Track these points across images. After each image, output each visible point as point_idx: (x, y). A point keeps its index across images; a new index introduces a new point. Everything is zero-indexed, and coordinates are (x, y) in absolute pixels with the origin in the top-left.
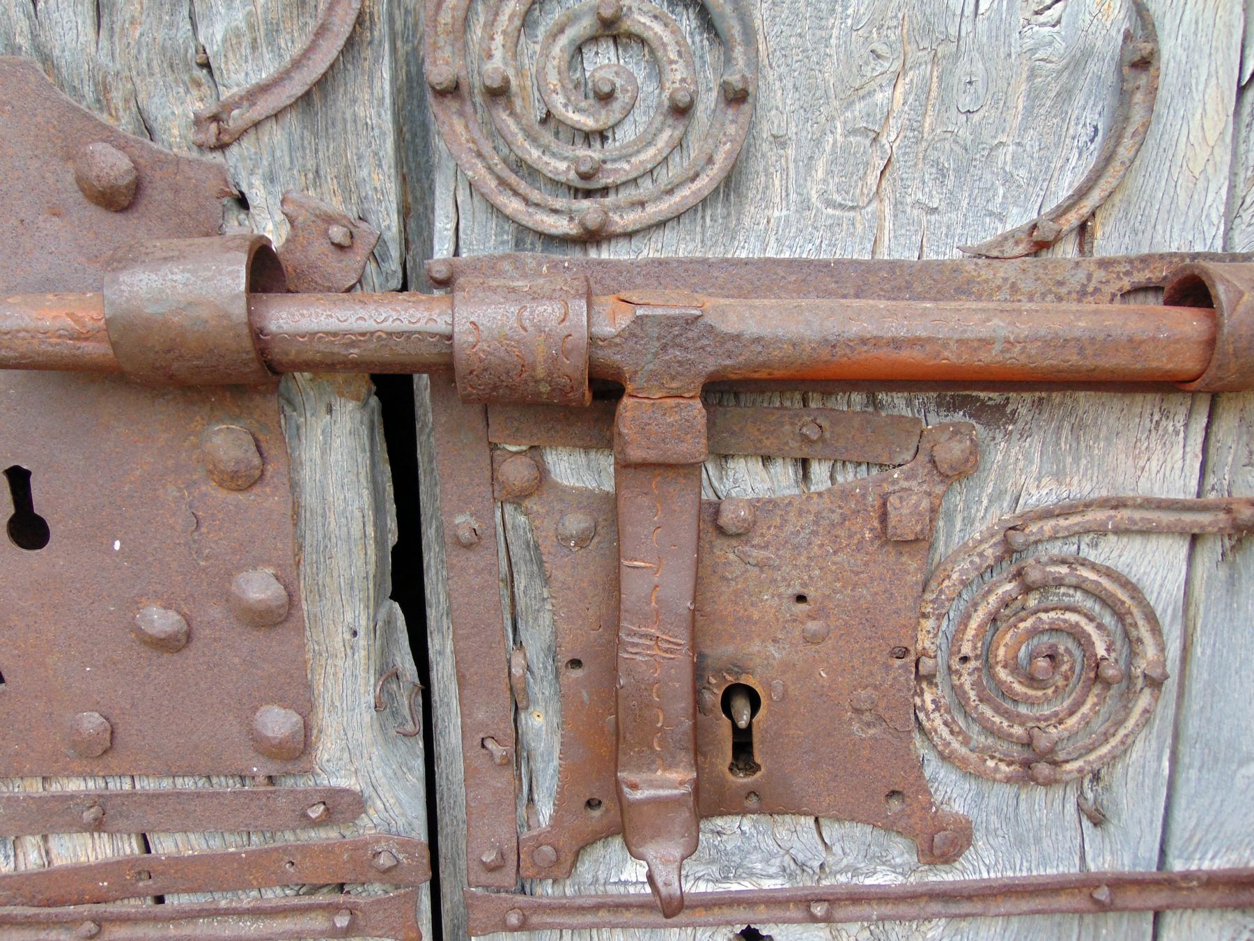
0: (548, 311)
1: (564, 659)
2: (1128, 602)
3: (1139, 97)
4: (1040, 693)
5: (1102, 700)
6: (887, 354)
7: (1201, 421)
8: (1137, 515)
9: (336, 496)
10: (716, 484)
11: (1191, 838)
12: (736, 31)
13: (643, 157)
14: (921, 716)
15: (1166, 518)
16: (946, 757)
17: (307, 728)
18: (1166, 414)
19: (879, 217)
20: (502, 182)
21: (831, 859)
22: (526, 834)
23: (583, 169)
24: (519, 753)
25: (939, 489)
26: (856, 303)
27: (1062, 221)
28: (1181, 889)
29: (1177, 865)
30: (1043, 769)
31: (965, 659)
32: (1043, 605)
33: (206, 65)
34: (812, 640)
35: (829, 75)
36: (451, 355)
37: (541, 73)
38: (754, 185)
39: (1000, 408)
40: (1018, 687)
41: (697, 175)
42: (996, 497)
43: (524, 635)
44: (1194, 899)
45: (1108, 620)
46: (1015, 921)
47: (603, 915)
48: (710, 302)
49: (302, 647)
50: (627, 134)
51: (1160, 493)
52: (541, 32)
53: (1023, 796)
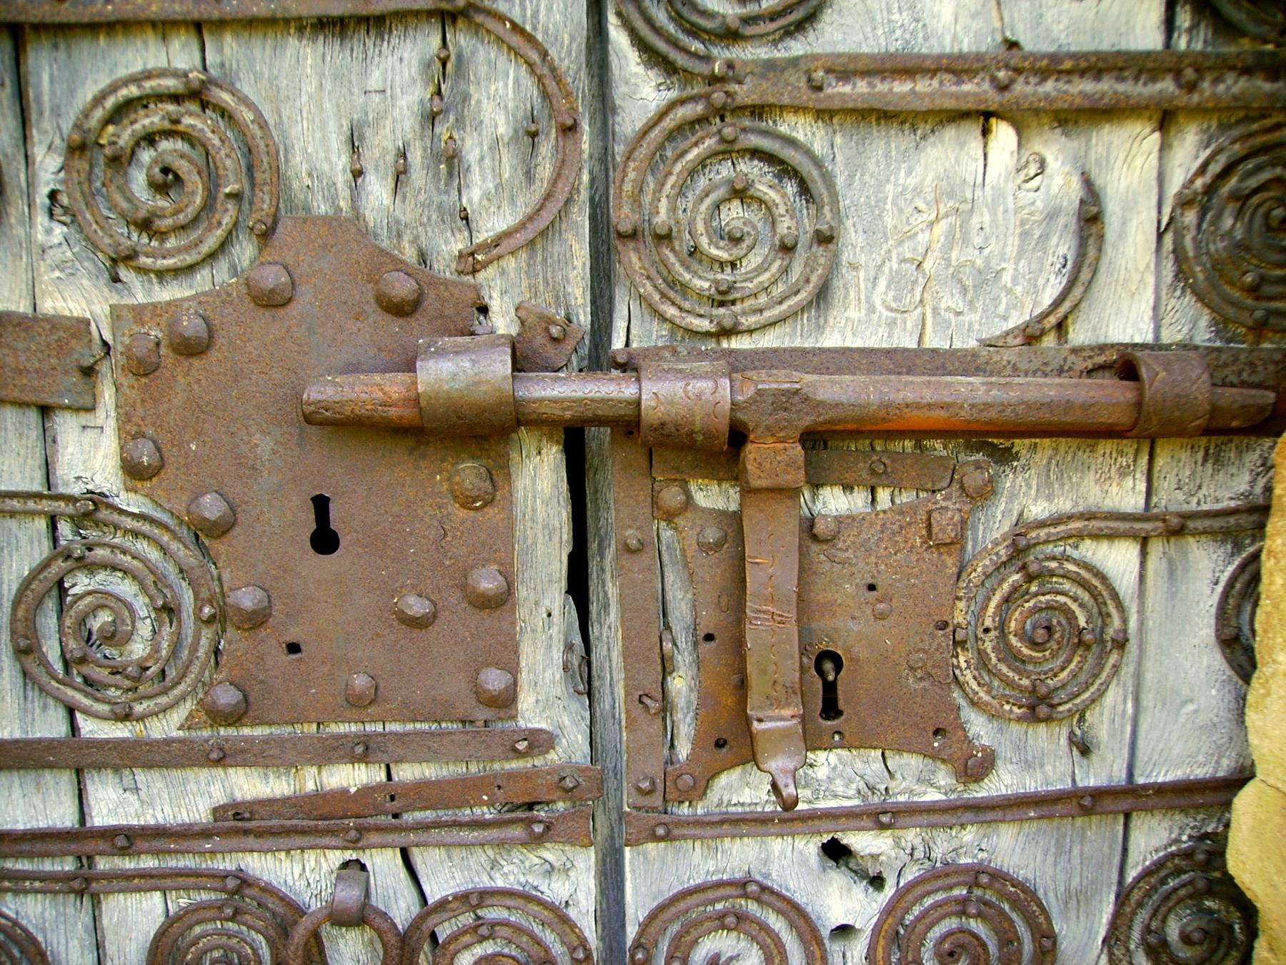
1: (701, 634)
2: (1100, 587)
3: (1091, 241)
4: (1040, 655)
5: (1084, 659)
7: (1144, 460)
8: (1102, 524)
10: (810, 505)
11: (1150, 759)
13: (761, 278)
14: (957, 672)
16: (974, 704)
17: (515, 684)
20: (663, 295)
21: (892, 784)
22: (670, 768)
23: (721, 288)
24: (666, 706)
25: (967, 508)
26: (910, 378)
27: (1045, 322)
28: (1141, 796)
29: (1140, 780)
30: (1043, 710)
31: (987, 630)
32: (1042, 590)
33: (466, 218)
34: (880, 617)
35: (889, 221)
36: (639, 415)
37: (692, 223)
38: (837, 294)
39: (1009, 449)
40: (1025, 651)
41: (798, 291)
44: (1150, 803)
45: (1086, 597)
49: (514, 624)
53: (1030, 732)
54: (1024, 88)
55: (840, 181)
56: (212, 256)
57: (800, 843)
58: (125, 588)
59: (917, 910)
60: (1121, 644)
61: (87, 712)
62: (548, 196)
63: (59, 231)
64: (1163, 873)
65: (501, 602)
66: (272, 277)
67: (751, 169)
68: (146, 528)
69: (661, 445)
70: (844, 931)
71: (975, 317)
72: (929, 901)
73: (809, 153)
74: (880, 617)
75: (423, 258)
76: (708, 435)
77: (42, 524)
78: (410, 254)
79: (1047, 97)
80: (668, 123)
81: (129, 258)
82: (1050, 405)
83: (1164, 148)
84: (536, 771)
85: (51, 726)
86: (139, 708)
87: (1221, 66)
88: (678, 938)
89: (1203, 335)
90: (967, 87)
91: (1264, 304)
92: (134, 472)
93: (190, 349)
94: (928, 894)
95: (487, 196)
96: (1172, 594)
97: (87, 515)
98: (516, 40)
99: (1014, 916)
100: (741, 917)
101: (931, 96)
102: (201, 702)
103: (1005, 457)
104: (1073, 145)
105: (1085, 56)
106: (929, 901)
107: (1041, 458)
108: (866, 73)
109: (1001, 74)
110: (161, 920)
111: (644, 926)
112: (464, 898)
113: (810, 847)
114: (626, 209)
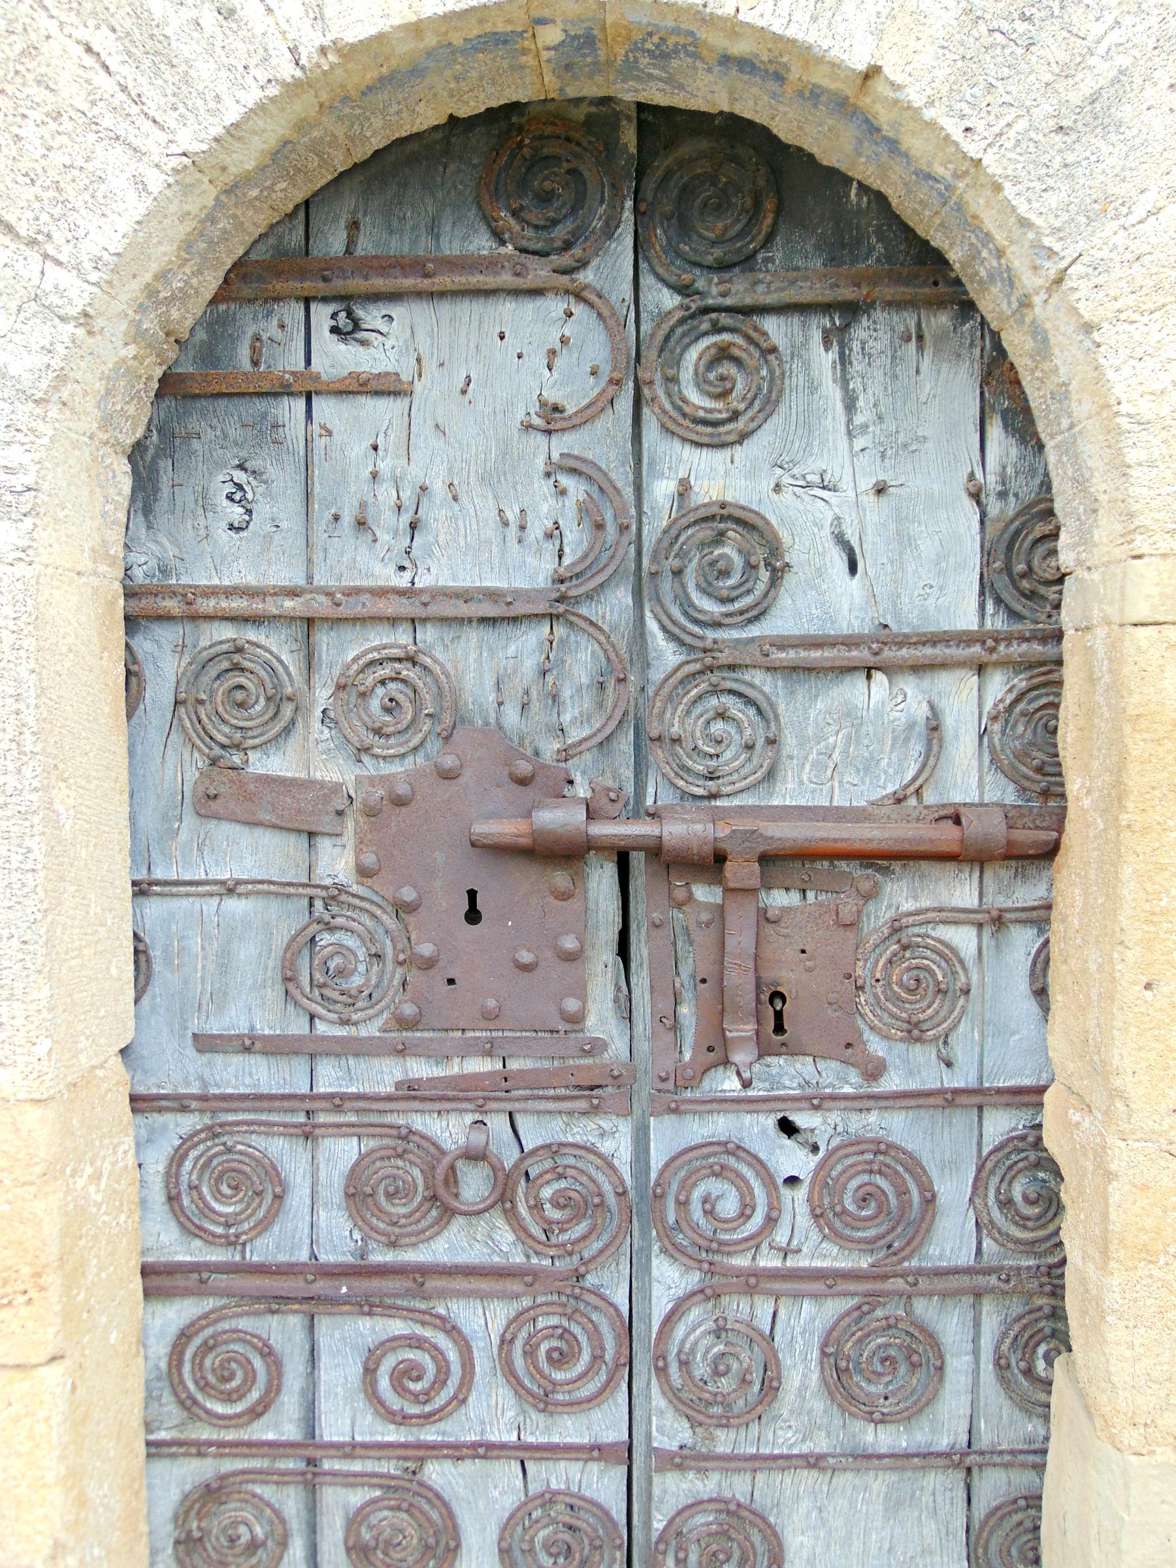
0: (699, 827)
6: (831, 845)
7: (976, 874)
9: (603, 905)
12: (771, 716)
15: (963, 916)
18: (960, 871)
19: (832, 787)
20: (677, 774)
24: (676, 1027)
29: (986, 1085)
34: (809, 970)
35: (810, 731)
38: (780, 776)
39: (887, 868)
42: (889, 907)
43: (681, 969)
45: (943, 964)
46: (911, 1113)
47: (715, 1106)
48: (761, 824)
50: (728, 755)
51: (961, 905)
52: (693, 715)
54: (888, 654)
57: (762, 1118)
59: (839, 1168)
64: (1007, 1150)
66: (449, 761)
67: (728, 701)
68: (367, 905)
69: (675, 863)
70: (792, 1181)
75: (537, 754)
77: (306, 901)
79: (903, 658)
81: (367, 750)
82: (910, 841)
85: (299, 1027)
86: (355, 1017)
87: (1009, 638)
89: (1010, 797)
90: (854, 653)
91: (1048, 778)
92: (364, 872)
93: (400, 802)
94: (847, 1156)
97: (333, 898)
99: (907, 1176)
101: (833, 659)
105: (924, 634)
108: (794, 646)
109: (874, 646)
110: (355, 1157)
111: (662, 1173)
113: (771, 1122)
114: (655, 724)
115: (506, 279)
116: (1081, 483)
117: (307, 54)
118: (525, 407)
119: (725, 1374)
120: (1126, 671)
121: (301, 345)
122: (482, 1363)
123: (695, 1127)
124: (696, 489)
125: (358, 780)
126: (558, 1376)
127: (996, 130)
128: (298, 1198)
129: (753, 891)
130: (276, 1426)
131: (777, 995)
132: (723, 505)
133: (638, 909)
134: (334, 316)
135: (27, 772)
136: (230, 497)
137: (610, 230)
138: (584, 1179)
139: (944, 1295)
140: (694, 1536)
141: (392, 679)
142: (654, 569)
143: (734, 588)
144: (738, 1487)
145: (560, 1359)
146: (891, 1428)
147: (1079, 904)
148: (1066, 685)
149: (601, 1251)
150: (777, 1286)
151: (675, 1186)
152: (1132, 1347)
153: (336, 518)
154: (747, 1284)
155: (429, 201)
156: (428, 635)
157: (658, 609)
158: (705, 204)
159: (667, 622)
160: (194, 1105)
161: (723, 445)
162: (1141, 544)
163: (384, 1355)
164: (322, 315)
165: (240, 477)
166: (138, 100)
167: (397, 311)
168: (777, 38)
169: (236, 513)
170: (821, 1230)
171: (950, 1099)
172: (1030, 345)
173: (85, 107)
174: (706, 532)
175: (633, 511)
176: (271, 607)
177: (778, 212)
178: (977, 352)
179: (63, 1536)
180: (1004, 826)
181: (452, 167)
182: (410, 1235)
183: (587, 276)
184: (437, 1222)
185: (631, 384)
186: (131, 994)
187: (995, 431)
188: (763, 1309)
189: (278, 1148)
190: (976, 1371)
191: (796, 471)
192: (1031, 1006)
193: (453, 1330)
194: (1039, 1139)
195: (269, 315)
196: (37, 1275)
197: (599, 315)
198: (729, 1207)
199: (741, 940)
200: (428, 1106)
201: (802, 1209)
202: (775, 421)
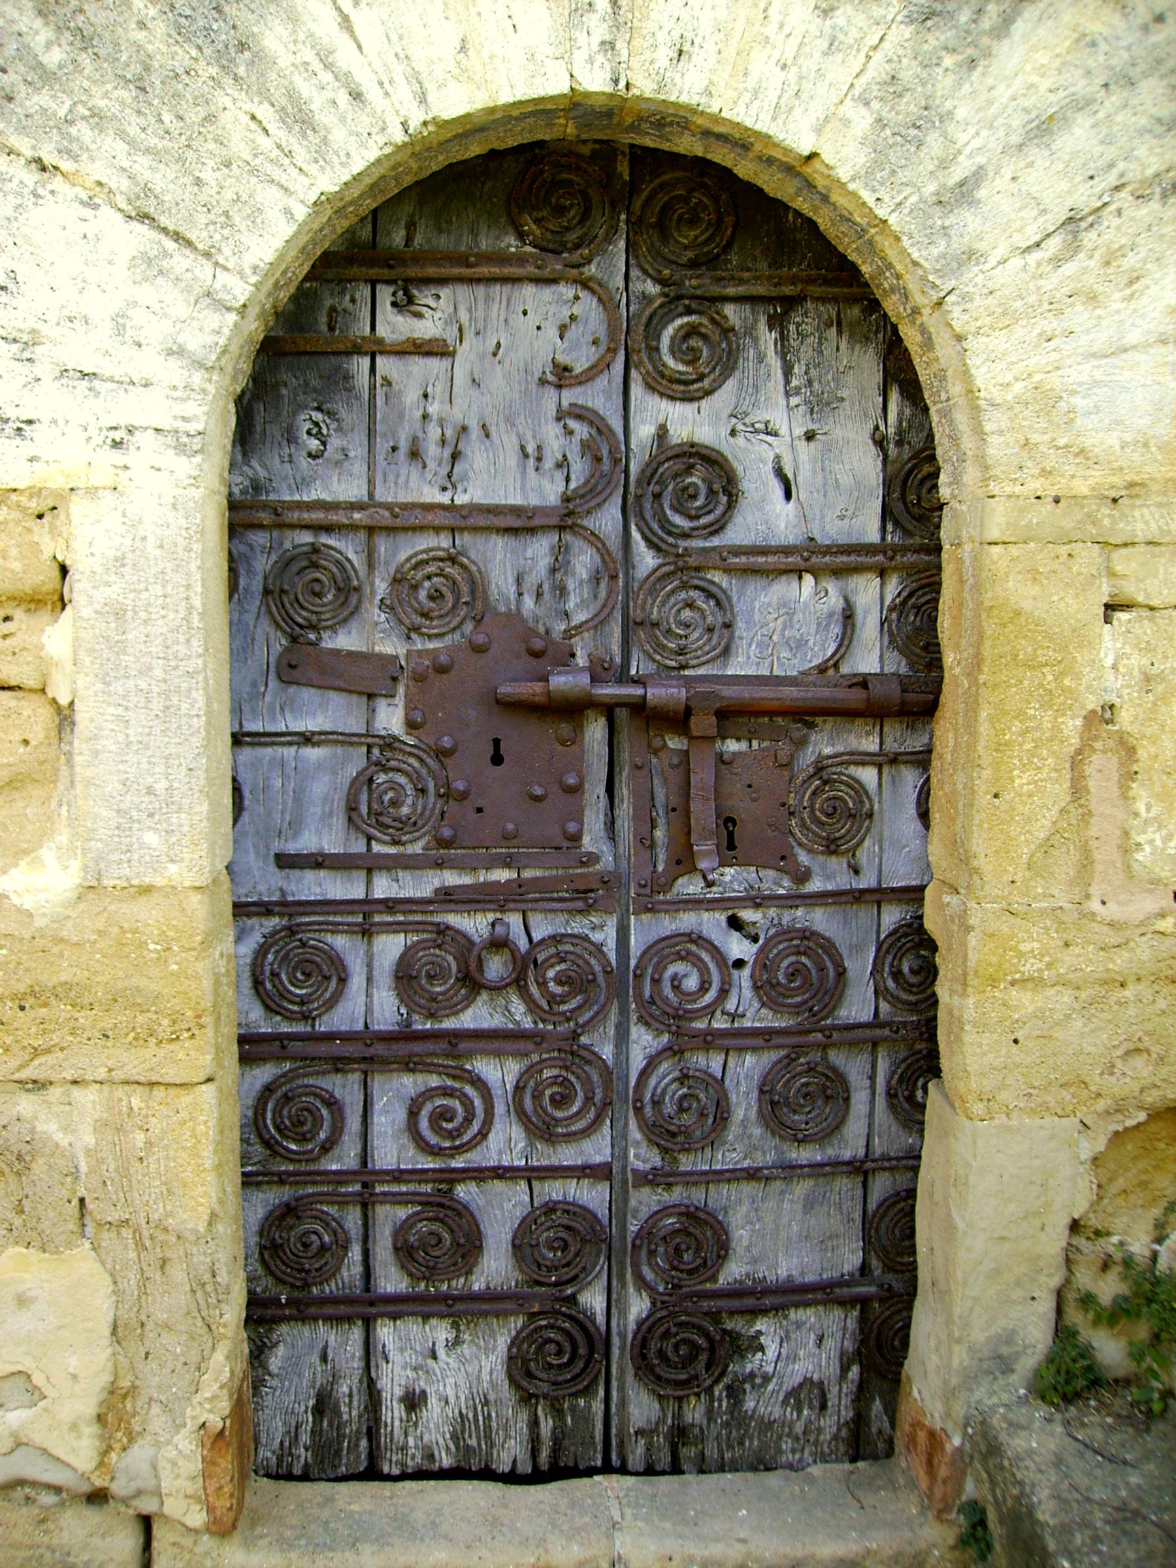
7: (878, 728)
16: (800, 844)
24: (652, 846)
35: (757, 617)
38: (733, 650)
55: (735, 599)
56: (454, 629)
57: (717, 915)
58: (403, 780)
60: (870, 815)
61: (378, 840)
62: (604, 606)
63: (383, 617)
65: (575, 790)
66: (480, 639)
67: (693, 594)
70: (739, 964)
71: (796, 661)
72: (781, 947)
73: (720, 587)
74: (754, 800)
75: (547, 632)
76: (675, 712)
77: (365, 749)
78: (542, 630)
80: (658, 574)
81: (416, 629)
82: (826, 699)
83: (882, 585)
84: (591, 874)
85: (359, 847)
86: (404, 838)
87: (905, 549)
88: (658, 963)
89: (903, 670)
93: (442, 670)
95: (577, 605)
96: (894, 792)
98: (592, 538)
100: (689, 953)
102: (435, 837)
103: (811, 726)
104: (840, 583)
106: (781, 947)
107: (828, 726)
108: (745, 554)
112: (553, 937)
113: (722, 917)
115: (531, 270)
116: (955, 439)
117: (414, 125)
118: (541, 364)
119: (686, 1110)
120: (984, 575)
121: (368, 315)
122: (500, 1108)
123: (666, 923)
124: (671, 432)
125: (409, 654)
126: (559, 1114)
127: (897, 200)
128: (357, 982)
129: (712, 739)
130: (339, 1159)
131: (730, 820)
132: (692, 445)
133: (625, 756)
134: (394, 294)
135: (195, 643)
136: (309, 433)
137: (609, 239)
138: (581, 962)
139: (851, 1044)
140: (662, 1233)
141: (437, 575)
142: (639, 492)
143: (701, 508)
144: (697, 1195)
145: (560, 1101)
146: (811, 1146)
147: (951, 744)
148: (944, 586)
149: (592, 1018)
150: (727, 1042)
151: (650, 971)
152: (980, 1045)
153: (394, 449)
154: (705, 1041)
155: (470, 211)
156: (465, 540)
157: (642, 524)
158: (680, 219)
159: (646, 531)
160: (277, 909)
161: (691, 400)
162: (994, 488)
163: (424, 1103)
164: (385, 294)
165: (318, 416)
166: (289, 154)
167: (445, 292)
168: (747, 129)
169: (314, 444)
170: (761, 999)
171: (858, 897)
172: (919, 338)
173: (249, 158)
174: (678, 466)
175: (623, 448)
176: (339, 517)
177: (735, 227)
178: (881, 336)
179: (217, 1208)
180: (899, 689)
181: (489, 185)
182: (445, 1008)
183: (592, 269)
184: (466, 998)
185: (623, 352)
186: (231, 822)
187: (894, 396)
188: (715, 1063)
189: (340, 942)
190: (872, 1101)
191: (747, 420)
192: (916, 825)
193: (478, 1082)
194: (921, 925)
195: (343, 293)
196: (199, 1017)
197: (600, 300)
198: (691, 983)
199: (702, 776)
200: (460, 907)
201: (746, 984)
202: (730, 385)
